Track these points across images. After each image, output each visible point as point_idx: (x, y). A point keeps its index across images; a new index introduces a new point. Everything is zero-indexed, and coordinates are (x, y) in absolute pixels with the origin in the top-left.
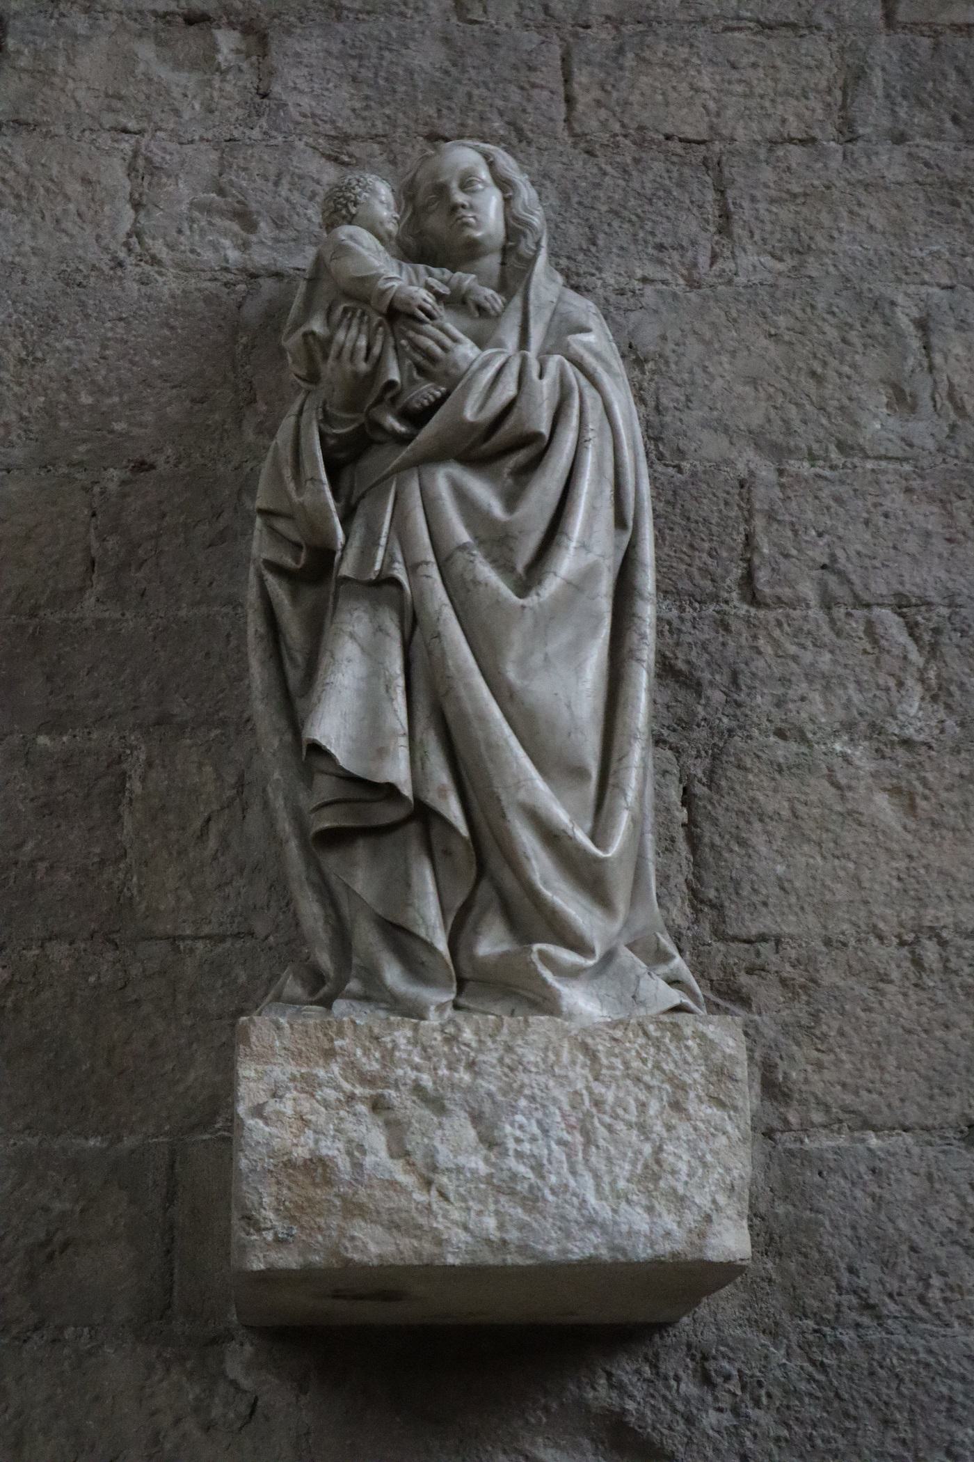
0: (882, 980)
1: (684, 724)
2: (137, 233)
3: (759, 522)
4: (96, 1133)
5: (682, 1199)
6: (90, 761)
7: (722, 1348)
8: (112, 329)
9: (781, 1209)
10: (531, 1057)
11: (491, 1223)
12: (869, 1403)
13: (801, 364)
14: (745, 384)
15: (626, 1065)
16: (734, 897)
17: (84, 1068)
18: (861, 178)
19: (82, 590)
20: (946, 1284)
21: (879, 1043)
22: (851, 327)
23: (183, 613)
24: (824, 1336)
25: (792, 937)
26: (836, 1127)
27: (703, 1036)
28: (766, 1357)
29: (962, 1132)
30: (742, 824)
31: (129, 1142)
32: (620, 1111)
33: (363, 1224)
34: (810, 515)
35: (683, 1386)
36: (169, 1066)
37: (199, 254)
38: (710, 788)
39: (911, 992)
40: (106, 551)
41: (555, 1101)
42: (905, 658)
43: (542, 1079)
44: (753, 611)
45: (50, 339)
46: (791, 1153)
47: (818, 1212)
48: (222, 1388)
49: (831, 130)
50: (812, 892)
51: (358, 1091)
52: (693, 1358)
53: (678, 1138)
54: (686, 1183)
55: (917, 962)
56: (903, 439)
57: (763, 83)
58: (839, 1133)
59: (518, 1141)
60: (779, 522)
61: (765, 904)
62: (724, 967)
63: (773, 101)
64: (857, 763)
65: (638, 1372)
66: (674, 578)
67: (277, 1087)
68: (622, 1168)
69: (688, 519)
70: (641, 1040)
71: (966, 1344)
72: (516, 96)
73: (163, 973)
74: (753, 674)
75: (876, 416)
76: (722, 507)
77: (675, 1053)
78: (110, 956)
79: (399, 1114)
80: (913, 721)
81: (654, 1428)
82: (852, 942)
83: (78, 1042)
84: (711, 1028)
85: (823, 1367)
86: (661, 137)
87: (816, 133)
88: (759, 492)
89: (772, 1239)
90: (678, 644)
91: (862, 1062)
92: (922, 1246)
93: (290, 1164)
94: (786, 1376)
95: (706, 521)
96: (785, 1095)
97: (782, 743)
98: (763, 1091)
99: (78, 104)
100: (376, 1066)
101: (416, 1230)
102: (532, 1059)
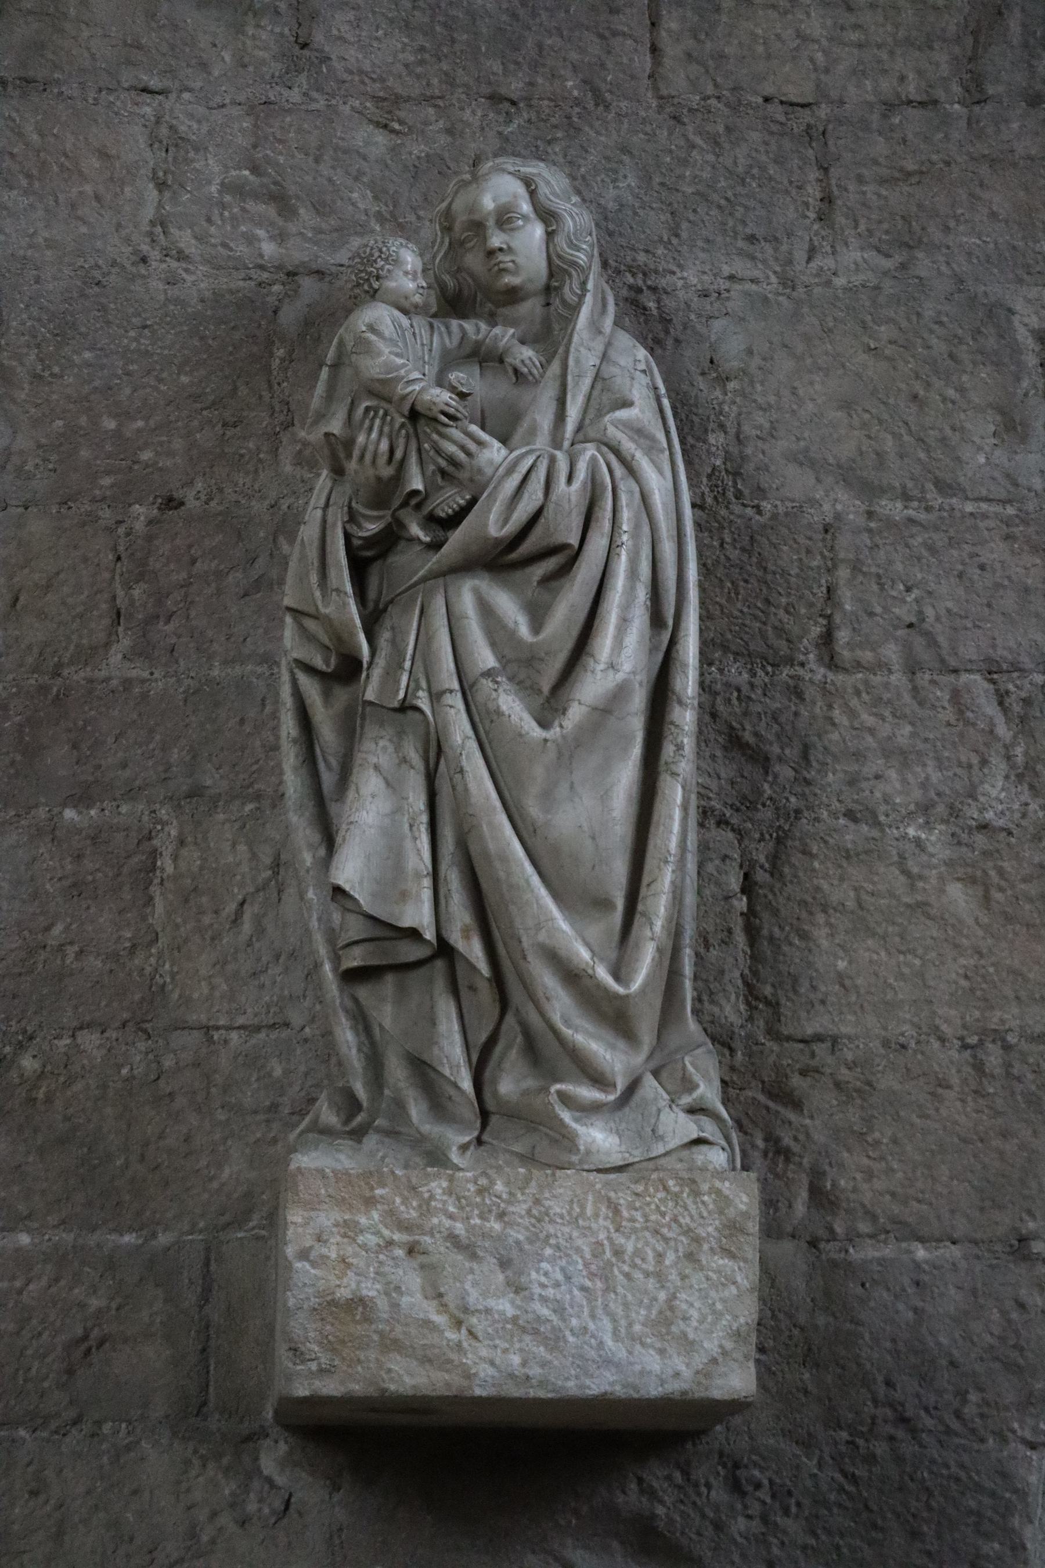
0: (940, 1085)
1: (748, 803)
2: (161, 222)
3: (843, 573)
4: (131, 1229)
5: (692, 1343)
6: (120, 836)
7: (754, 1457)
8: (136, 339)
9: (821, 1320)
10: (557, 1208)
11: (516, 1360)
12: (898, 1516)
13: (903, 386)
14: (840, 408)
15: (646, 1216)
16: (791, 994)
17: (118, 1163)
18: (986, 152)
19: (107, 645)
20: (983, 1399)
21: (932, 1151)
22: (961, 341)
23: (216, 673)
24: (858, 1448)
25: (849, 1038)
26: (883, 1237)
27: (719, 1192)
28: (798, 1467)
29: (1011, 1246)
30: (804, 915)
31: (164, 1239)
32: (638, 1261)
33: (398, 1358)
34: (899, 567)
35: (713, 1493)
36: (203, 1163)
37: (231, 250)
38: (772, 875)
39: (969, 1099)
40: (132, 602)
41: (578, 1250)
42: (992, 732)
43: (567, 1230)
44: (831, 676)
45: (67, 350)
46: (834, 1264)
47: (857, 1324)
48: (256, 1484)
49: (956, 89)
50: (873, 990)
51: (397, 1237)
52: (724, 1466)
53: (691, 1287)
54: (696, 1329)
55: (979, 1067)
56: (1008, 476)
57: (881, 30)
58: (885, 1242)
59: (543, 1286)
60: (865, 574)
61: (823, 1002)
62: (776, 1067)
63: (892, 53)
64: (931, 849)
65: (669, 1478)
66: (746, 637)
67: (322, 1232)
68: (638, 1313)
69: (765, 569)
70: (661, 1195)
71: (999, 1461)
72: (595, 48)
73: (196, 1065)
74: (825, 748)
75: (980, 449)
76: (803, 556)
77: (692, 1207)
78: (142, 1046)
79: (434, 1259)
80: (994, 804)
81: (683, 1533)
82: (913, 1044)
83: (112, 1136)
84: (727, 1184)
85: (854, 1479)
86: (760, 100)
87: (940, 94)
88: (844, 541)
89: (810, 1349)
90: (746, 713)
91: (914, 1171)
92: (962, 1360)
93: (333, 1303)
94: (816, 1486)
95: (785, 573)
96: (831, 1203)
97: (852, 826)
98: (810, 1198)
99: (93, 56)
100: (414, 1214)
101: (445, 1364)
102: (558, 1210)
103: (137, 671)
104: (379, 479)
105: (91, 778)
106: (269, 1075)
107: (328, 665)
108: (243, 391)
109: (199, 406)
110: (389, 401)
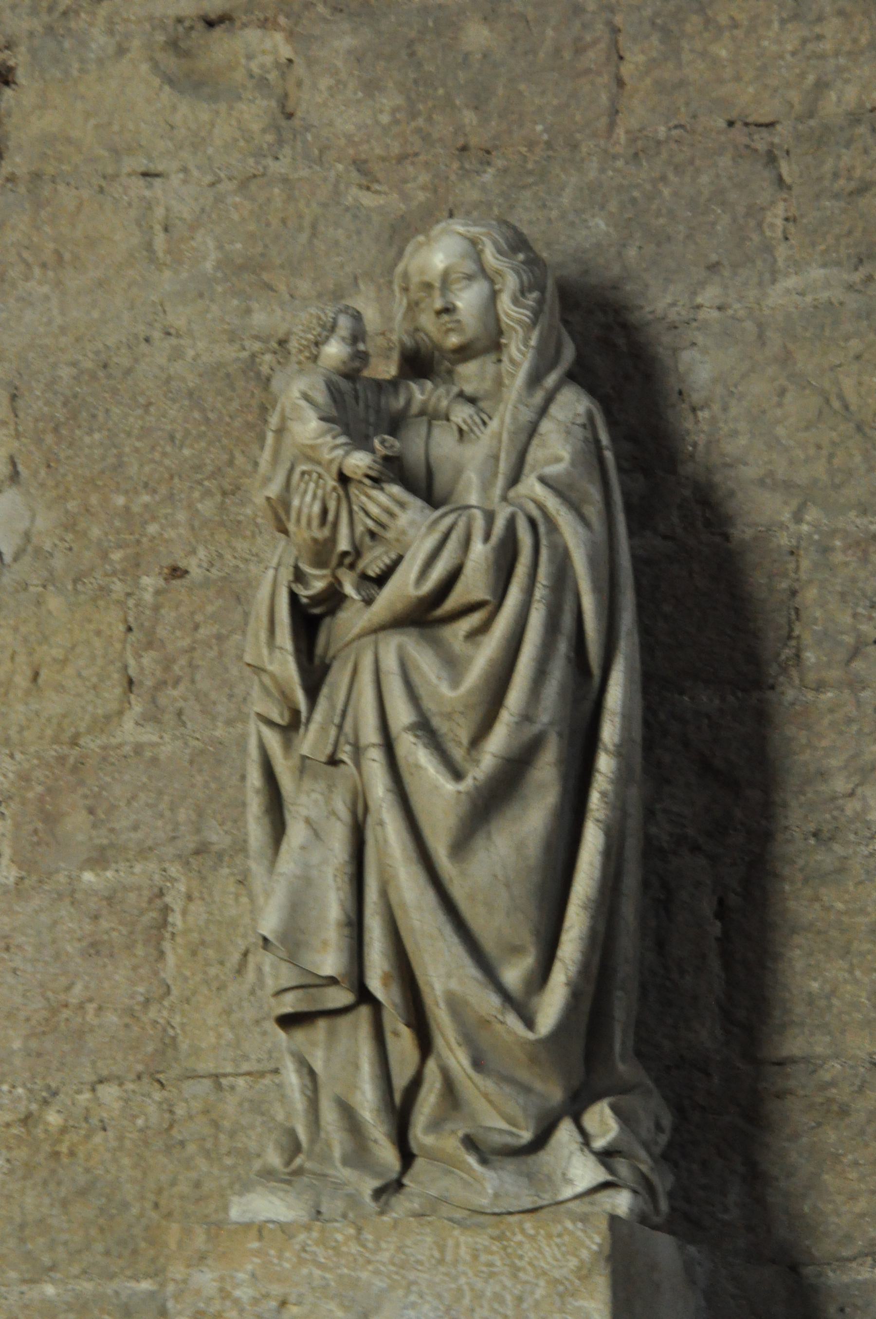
4: (147, 1276)
6: (132, 896)
19: (120, 713)
40: (142, 669)
78: (157, 1096)
103: (148, 735)
104: (315, 541)
105: (105, 842)
106: (273, 1119)
107: (283, 720)
108: (240, 460)
109: (199, 476)
110: (319, 463)
